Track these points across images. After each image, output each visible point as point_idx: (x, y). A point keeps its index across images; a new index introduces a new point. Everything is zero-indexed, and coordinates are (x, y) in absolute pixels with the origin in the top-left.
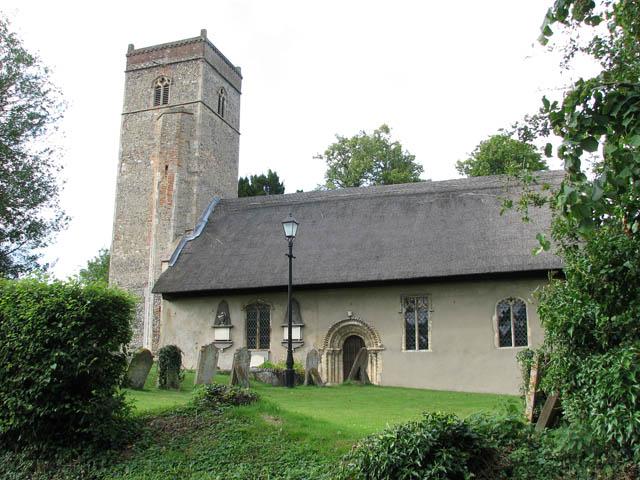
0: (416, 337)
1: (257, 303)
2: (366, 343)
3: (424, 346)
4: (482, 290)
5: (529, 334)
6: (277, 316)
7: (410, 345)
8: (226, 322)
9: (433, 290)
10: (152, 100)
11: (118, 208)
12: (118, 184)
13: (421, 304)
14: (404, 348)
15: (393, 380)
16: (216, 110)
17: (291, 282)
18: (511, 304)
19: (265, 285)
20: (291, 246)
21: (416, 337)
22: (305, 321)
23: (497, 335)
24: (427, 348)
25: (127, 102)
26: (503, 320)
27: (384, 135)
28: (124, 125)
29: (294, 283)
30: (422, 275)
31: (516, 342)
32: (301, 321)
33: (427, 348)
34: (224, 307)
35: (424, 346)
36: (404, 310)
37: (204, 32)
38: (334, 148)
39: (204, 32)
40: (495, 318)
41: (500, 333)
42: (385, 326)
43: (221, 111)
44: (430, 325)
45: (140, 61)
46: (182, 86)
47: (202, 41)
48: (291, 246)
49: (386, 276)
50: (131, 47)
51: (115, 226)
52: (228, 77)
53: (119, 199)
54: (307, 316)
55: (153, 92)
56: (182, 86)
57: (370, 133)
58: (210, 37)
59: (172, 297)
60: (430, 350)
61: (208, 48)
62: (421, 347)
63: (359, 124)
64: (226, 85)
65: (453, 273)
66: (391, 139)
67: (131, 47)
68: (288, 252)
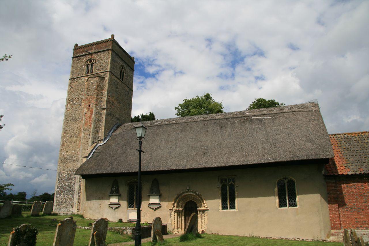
14: (220, 208)
20: (141, 144)
22: (162, 192)
24: (234, 208)
29: (143, 170)
31: (289, 204)
33: (234, 208)
39: (113, 36)
43: (122, 77)
50: (76, 45)
62: (290, 205)
64: (125, 65)
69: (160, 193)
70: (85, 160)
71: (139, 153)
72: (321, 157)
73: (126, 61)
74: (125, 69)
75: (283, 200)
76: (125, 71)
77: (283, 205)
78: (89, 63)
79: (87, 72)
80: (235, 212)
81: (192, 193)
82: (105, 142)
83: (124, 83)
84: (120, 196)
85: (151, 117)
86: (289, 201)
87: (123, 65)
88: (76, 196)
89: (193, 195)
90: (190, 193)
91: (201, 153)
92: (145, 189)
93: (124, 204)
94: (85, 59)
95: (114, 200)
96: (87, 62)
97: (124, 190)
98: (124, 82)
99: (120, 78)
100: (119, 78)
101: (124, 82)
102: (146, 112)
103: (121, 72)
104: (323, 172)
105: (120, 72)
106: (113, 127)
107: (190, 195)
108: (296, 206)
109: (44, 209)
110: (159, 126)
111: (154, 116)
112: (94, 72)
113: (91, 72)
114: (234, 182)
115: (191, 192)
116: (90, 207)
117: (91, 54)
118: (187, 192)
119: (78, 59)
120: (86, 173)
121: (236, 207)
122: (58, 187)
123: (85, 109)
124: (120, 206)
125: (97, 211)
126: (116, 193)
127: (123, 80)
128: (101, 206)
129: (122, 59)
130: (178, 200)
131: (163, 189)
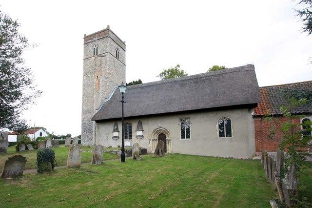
0: (185, 133)
1: (126, 122)
2: (167, 136)
3: (188, 137)
4: (211, 115)
5: (232, 132)
6: (134, 126)
7: (183, 137)
8: (117, 130)
9: (192, 116)
10: (93, 53)
11: (83, 92)
12: (83, 84)
13: (186, 121)
14: (180, 138)
15: (176, 151)
16: (115, 56)
17: (123, 116)
18: (224, 120)
19: (128, 116)
20: (123, 97)
21: (185, 133)
22: (144, 129)
23: (218, 133)
24: (189, 138)
25: (85, 55)
26: (221, 126)
27: (178, 68)
28: (84, 64)
29: (125, 116)
30: (187, 110)
31: (226, 135)
32: (142, 129)
33: (189, 138)
34: (116, 125)
35: (188, 137)
36: (180, 124)
37: (108, 26)
38: (162, 73)
39: (108, 26)
40: (217, 126)
41: (220, 131)
42: (173, 127)
43: (117, 56)
44: (190, 129)
45: (88, 39)
46: (103, 45)
47: (108, 30)
48: (123, 97)
49: (173, 110)
50: (85, 35)
51: (83, 98)
52: (121, 45)
53: (84, 89)
54: (144, 126)
55: (93, 51)
56: (103, 45)
57: (174, 68)
58: (111, 28)
59: (99, 122)
60: (191, 139)
61: (110, 32)
62: (187, 138)
63: (171, 65)
64: (119, 48)
65: (200, 108)
66: (180, 69)
67: (85, 35)
68: (121, 99)
70: (97, 111)
72: (251, 103)
85: (140, 82)
88: (94, 133)
91: (6, 100)
101: (119, 59)
102: (137, 80)
104: (253, 113)
109: (225, 131)
110: (143, 88)
111: (141, 82)
112: (99, 54)
117: (95, 41)
125: (106, 141)
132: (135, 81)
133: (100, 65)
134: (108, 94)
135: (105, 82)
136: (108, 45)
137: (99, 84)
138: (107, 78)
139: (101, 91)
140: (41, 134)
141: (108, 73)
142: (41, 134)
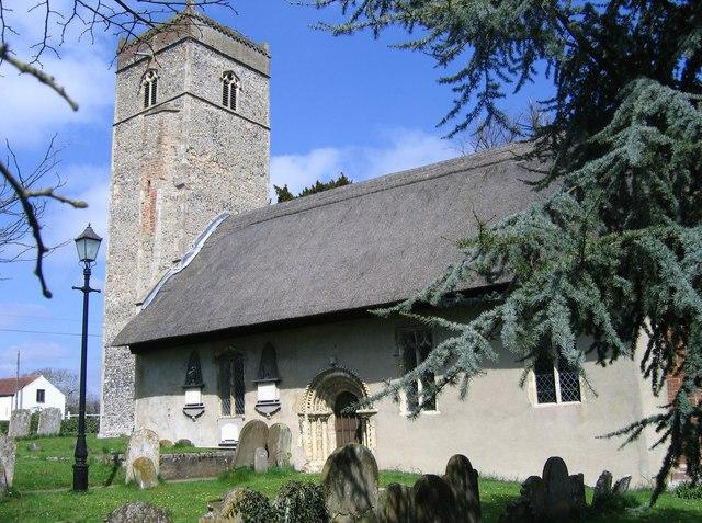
20: (87, 274)
22: (282, 373)
31: (563, 394)
34: (195, 361)
48: (87, 274)
62: (565, 398)
64: (238, 69)
69: (277, 376)
71: (83, 293)
73: (239, 58)
74: (238, 79)
75: (548, 383)
76: (238, 84)
77: (546, 395)
78: (148, 79)
79: (146, 105)
80: (434, 417)
81: (342, 374)
82: (186, 265)
83: (238, 115)
84: (202, 388)
86: (562, 386)
87: (229, 69)
89: (345, 378)
90: (338, 374)
92: (251, 367)
93: (213, 402)
94: (139, 71)
95: (193, 396)
96: (143, 77)
97: (210, 373)
98: (237, 111)
99: (225, 103)
100: (220, 104)
101: (237, 111)
103: (226, 89)
105: (221, 89)
106: (211, 225)
107: (341, 377)
108: (540, 402)
113: (154, 102)
114: (431, 341)
115: (338, 370)
116: (151, 417)
117: (148, 58)
118: (333, 371)
119: (127, 73)
120: (132, 340)
121: (543, 405)
122: (106, 376)
123: (142, 192)
124: (279, 409)
126: (195, 382)
127: (233, 107)
128: (171, 413)
129: (224, 55)
130: (322, 387)
131: (283, 366)
132: (310, 188)
133: (160, 141)
134: (183, 245)
135: (173, 199)
136: (187, 67)
137: (152, 209)
138: (180, 187)
139: (158, 235)
140: (41, 396)
141: (184, 166)
142: (41, 396)
